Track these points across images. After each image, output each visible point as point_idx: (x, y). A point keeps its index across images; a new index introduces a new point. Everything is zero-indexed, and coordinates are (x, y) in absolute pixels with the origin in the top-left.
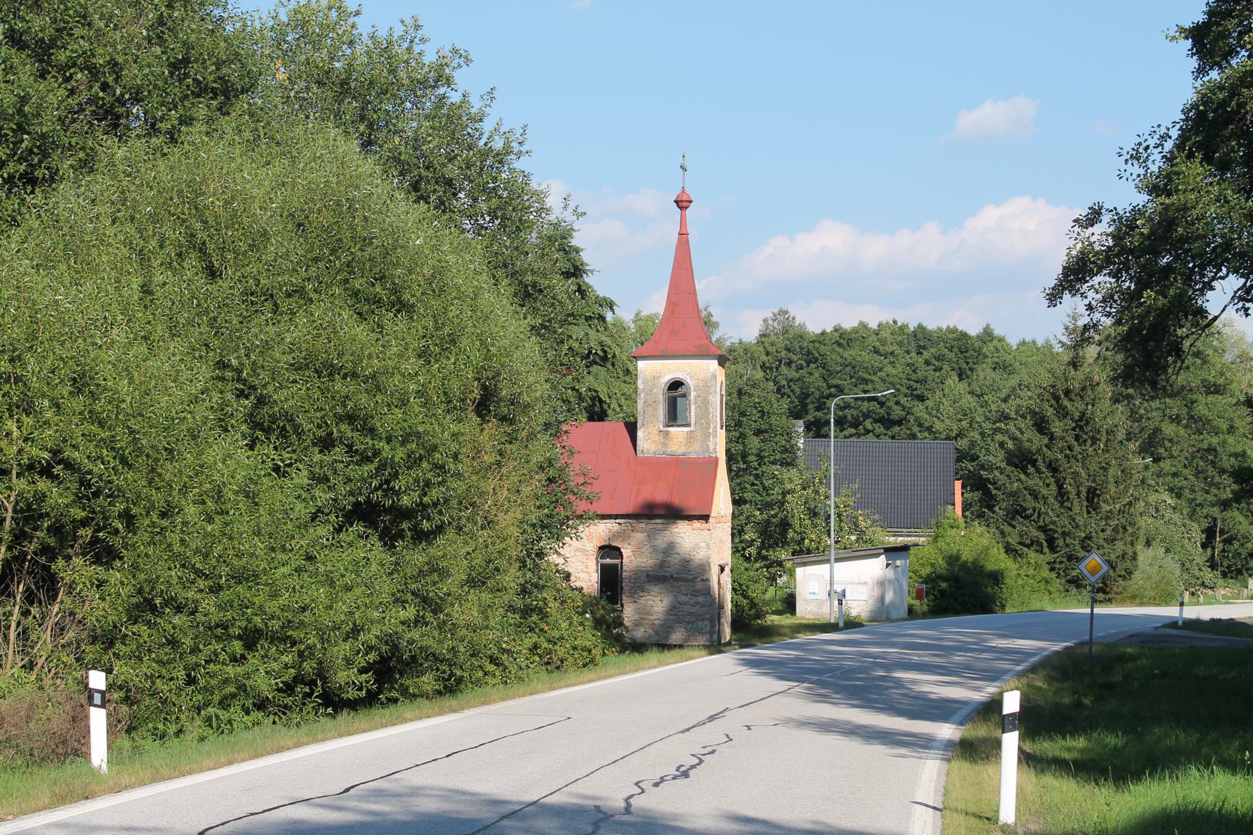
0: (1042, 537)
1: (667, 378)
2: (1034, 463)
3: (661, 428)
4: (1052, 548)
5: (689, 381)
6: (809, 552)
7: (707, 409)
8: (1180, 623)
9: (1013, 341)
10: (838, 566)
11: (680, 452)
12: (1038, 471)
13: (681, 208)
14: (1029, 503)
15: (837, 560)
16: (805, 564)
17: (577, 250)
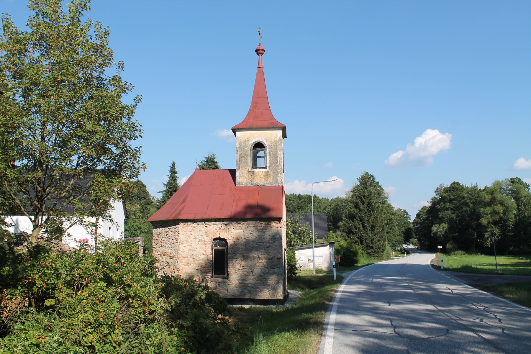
0: (359, 240)
1: (253, 141)
2: (355, 218)
3: (250, 170)
4: (362, 243)
5: (266, 143)
6: (294, 245)
7: (276, 158)
8: (442, 268)
9: (320, 198)
10: (316, 249)
11: (261, 183)
12: (357, 220)
13: (258, 54)
14: (354, 230)
15: (315, 247)
16: (299, 249)
17: (216, 162)
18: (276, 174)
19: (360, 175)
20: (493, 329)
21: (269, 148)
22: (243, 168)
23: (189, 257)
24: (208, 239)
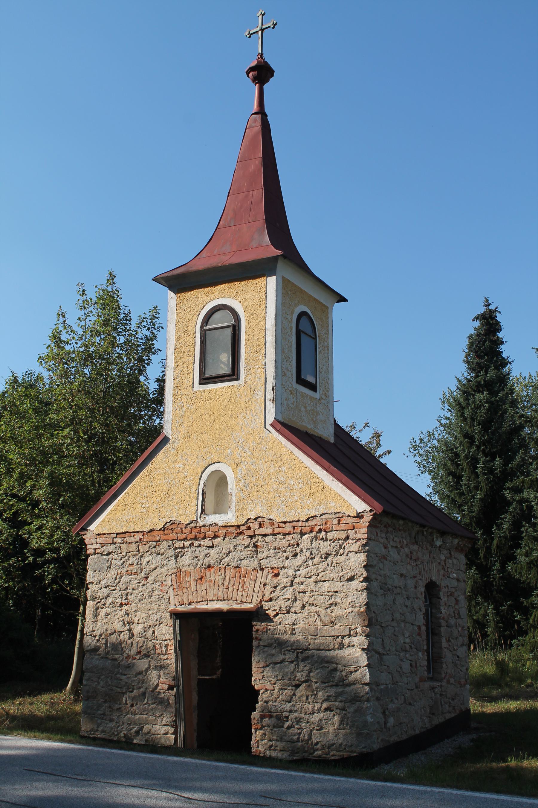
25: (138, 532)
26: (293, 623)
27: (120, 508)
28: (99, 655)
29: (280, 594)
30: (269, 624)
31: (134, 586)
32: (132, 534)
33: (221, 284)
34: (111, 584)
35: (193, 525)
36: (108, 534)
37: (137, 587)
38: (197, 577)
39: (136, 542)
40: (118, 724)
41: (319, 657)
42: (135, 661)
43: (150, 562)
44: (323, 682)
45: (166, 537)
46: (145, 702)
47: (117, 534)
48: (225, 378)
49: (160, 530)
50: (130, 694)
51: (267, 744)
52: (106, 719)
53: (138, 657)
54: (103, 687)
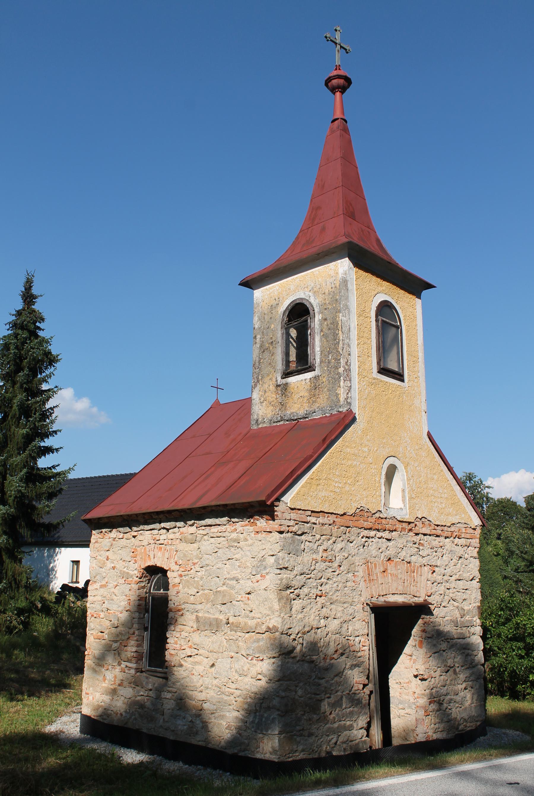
3: (280, 381)
11: (301, 413)
18: (335, 380)
19: (45, 315)
20: (163, 671)
21: (320, 312)
22: (266, 379)
23: (102, 615)
24: (135, 570)
25: (332, 513)
26: (444, 616)
27: (314, 481)
28: (294, 657)
29: (437, 590)
30: (431, 617)
31: (329, 575)
32: (326, 515)
33: (388, 282)
34: (307, 571)
35: (377, 515)
36: (303, 510)
37: (332, 576)
38: (382, 569)
39: (330, 525)
40: (317, 738)
41: (461, 644)
42: (333, 661)
43: (343, 550)
44: (462, 666)
45: (356, 524)
46: (344, 707)
47: (312, 512)
48: (397, 376)
49: (352, 515)
50: (330, 700)
51: (434, 728)
52: (304, 736)
53: (335, 656)
54: (300, 697)
